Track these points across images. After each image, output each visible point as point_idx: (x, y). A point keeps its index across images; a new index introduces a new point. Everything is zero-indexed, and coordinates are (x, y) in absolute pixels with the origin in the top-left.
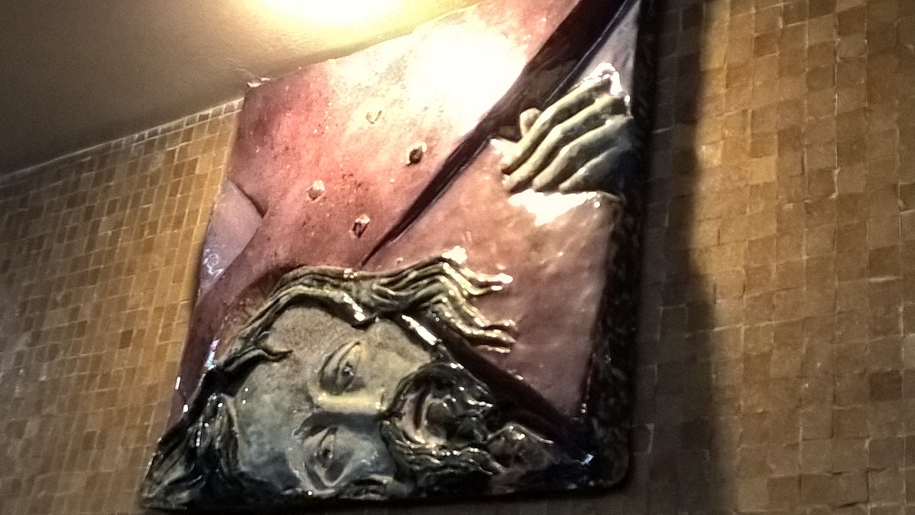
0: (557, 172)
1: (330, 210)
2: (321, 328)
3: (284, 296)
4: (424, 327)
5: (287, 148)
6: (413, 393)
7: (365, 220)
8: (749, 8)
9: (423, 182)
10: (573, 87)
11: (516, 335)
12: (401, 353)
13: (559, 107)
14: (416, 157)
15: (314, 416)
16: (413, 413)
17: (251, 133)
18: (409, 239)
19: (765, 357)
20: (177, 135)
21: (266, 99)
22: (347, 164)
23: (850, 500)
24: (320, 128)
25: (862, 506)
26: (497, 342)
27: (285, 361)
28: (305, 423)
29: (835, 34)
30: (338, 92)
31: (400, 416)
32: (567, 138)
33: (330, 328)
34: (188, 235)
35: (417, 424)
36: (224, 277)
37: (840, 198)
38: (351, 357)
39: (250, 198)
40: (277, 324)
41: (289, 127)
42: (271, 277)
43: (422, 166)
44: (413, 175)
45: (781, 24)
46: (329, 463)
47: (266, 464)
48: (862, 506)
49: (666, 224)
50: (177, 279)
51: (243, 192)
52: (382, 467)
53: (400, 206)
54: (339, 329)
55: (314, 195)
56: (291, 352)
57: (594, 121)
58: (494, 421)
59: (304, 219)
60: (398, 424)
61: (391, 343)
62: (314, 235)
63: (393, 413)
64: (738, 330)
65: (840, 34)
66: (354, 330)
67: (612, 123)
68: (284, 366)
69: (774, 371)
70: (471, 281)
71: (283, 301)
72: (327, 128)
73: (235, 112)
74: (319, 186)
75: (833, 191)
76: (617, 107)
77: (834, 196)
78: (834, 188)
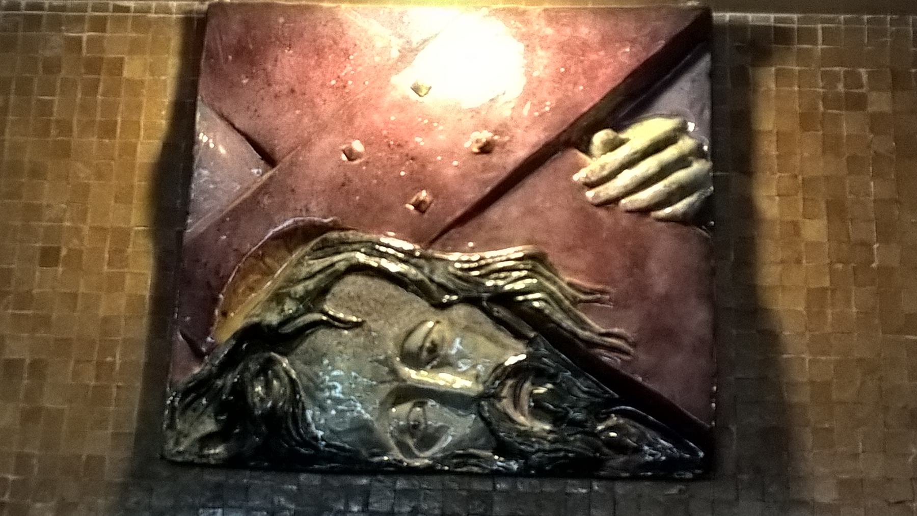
0: (654, 202)
1: (377, 177)
2: (394, 301)
3: (340, 260)
4: (392, 272)
5: (293, 91)
6: (512, 379)
7: (424, 195)
8: (791, 85)
9: (495, 176)
10: (642, 116)
11: (634, 345)
12: (490, 338)
13: (654, 140)
14: (488, 148)
15: (398, 389)
16: (285, 318)
17: (230, 57)
18: (480, 227)
19: (827, 384)
20: (81, 20)
21: (247, 25)
22: (392, 131)
23: (902, 499)
24: (339, 80)
25: (909, 504)
26: (613, 349)
27: (357, 330)
28: (390, 394)
29: (868, 130)
30: (362, 47)
31: (500, 399)
32: (664, 172)
33: (405, 302)
34: (128, 149)
35: (516, 404)
36: (228, 219)
37: (879, 268)
38: (434, 336)
39: (239, 131)
40: (336, 289)
41: (291, 67)
42: (300, 232)
43: (494, 159)
44: (484, 165)
45: (821, 109)
46: (419, 434)
47: (351, 430)
48: (909, 504)
49: (732, 257)
50: (123, 197)
51: (233, 125)
52: (482, 441)
53: (472, 195)
54: (416, 305)
55: (351, 155)
56: (363, 322)
57: (682, 162)
58: (598, 411)
59: (342, 180)
60: (498, 406)
61: (477, 327)
62: (359, 200)
63: (491, 396)
64: (803, 359)
65: (872, 130)
66: (432, 309)
67: (698, 167)
68: (357, 335)
69: (835, 396)
70: (570, 285)
71: (341, 266)
72: (350, 82)
73: (174, 16)
74: (358, 146)
75: (873, 262)
76: (698, 153)
77: (874, 265)
78: (873, 258)
